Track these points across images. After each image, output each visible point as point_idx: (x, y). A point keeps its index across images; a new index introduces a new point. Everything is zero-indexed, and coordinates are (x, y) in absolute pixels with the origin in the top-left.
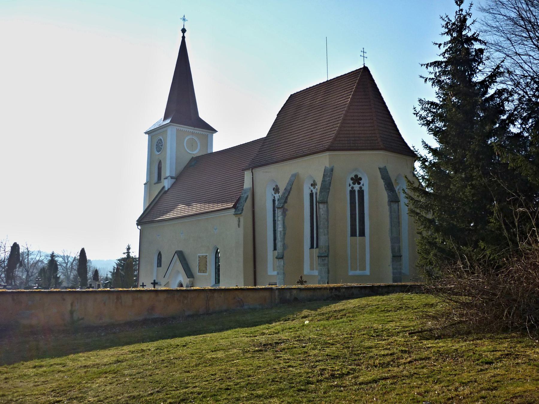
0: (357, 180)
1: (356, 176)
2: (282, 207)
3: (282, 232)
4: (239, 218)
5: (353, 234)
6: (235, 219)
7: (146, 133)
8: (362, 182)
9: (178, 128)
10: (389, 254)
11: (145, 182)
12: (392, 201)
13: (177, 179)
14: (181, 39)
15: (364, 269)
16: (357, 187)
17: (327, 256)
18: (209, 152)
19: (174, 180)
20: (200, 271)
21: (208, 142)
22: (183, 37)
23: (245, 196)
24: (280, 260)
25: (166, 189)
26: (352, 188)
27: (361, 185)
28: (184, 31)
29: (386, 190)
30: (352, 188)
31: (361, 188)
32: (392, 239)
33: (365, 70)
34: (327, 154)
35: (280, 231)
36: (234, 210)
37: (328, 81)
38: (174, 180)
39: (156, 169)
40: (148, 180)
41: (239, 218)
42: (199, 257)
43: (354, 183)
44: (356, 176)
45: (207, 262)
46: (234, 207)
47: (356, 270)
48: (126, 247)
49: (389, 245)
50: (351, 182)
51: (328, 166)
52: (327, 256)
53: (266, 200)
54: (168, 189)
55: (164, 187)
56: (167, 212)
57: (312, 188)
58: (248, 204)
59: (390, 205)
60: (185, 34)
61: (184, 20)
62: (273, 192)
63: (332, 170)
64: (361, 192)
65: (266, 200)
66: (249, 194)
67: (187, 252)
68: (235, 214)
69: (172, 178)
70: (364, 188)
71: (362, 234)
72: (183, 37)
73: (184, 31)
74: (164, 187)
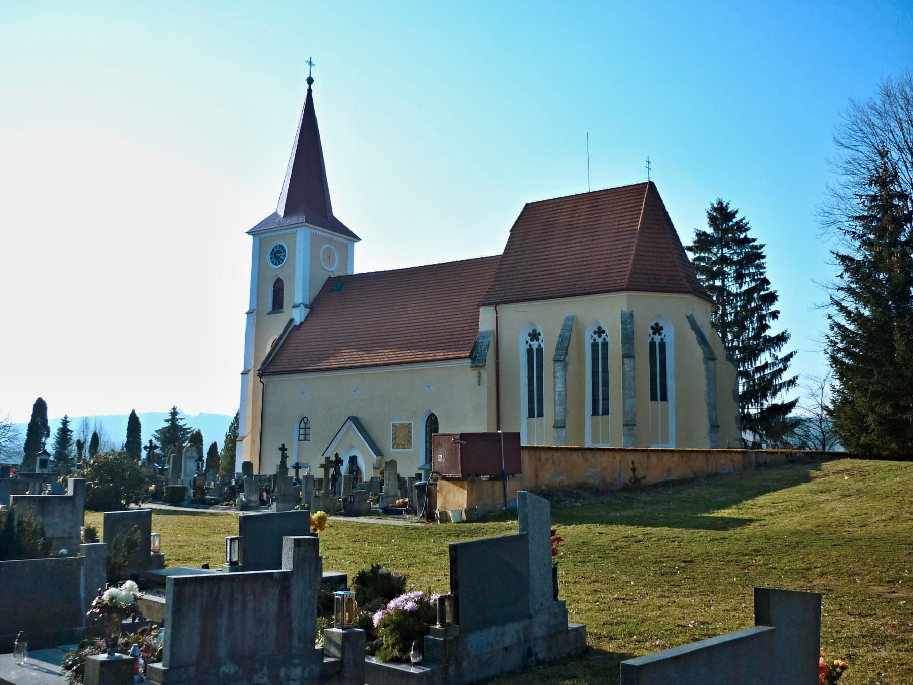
0: (657, 329)
1: (657, 324)
2: (564, 360)
3: (563, 393)
4: (479, 373)
5: (654, 398)
6: (473, 375)
7: (248, 233)
8: (664, 332)
9: (313, 231)
10: (705, 425)
11: (247, 309)
12: (627, 357)
13: (313, 307)
14: (306, 93)
15: (666, 441)
16: (657, 339)
17: (564, 427)
18: (349, 273)
19: (308, 310)
20: (395, 445)
21: (347, 257)
22: (310, 91)
23: (486, 341)
24: (559, 430)
25: (297, 322)
26: (653, 339)
27: (662, 336)
28: (310, 81)
29: (700, 344)
30: (653, 339)
31: (662, 340)
32: (708, 405)
33: (652, 185)
34: (624, 295)
35: (560, 392)
36: (470, 361)
37: (589, 193)
38: (308, 310)
39: (270, 294)
40: (255, 306)
41: (479, 373)
42: (393, 425)
43: (654, 334)
44: (657, 324)
45: (410, 432)
46: (470, 357)
47: (598, 443)
48: (171, 410)
49: (704, 411)
50: (651, 332)
51: (625, 309)
52: (564, 427)
53: (516, 346)
54: (301, 323)
55: (292, 320)
56: (327, 358)
57: (596, 336)
58: (490, 354)
59: (706, 363)
60: (312, 86)
61: (311, 63)
62: (528, 339)
63: (632, 315)
64: (663, 345)
65: (516, 346)
66: (492, 339)
67: (365, 417)
68: (474, 367)
69: (306, 307)
70: (666, 340)
71: (664, 398)
72: (310, 91)
73: (310, 81)
74: (292, 320)
